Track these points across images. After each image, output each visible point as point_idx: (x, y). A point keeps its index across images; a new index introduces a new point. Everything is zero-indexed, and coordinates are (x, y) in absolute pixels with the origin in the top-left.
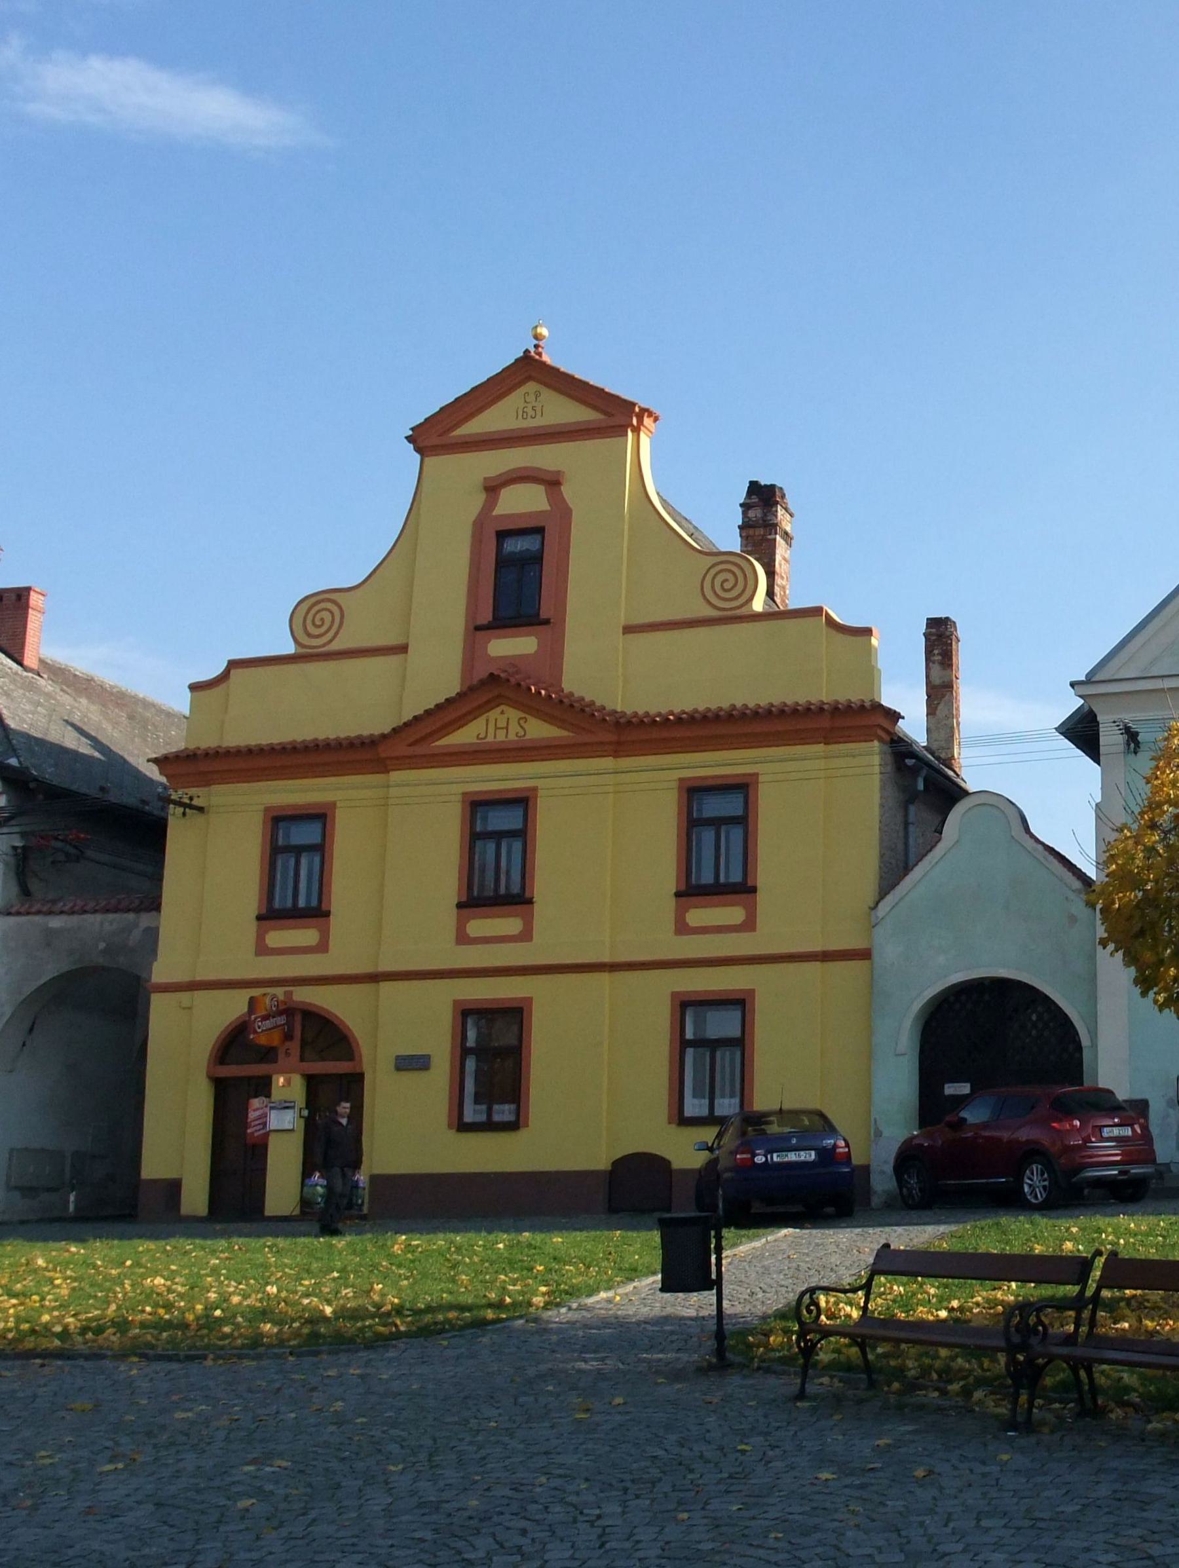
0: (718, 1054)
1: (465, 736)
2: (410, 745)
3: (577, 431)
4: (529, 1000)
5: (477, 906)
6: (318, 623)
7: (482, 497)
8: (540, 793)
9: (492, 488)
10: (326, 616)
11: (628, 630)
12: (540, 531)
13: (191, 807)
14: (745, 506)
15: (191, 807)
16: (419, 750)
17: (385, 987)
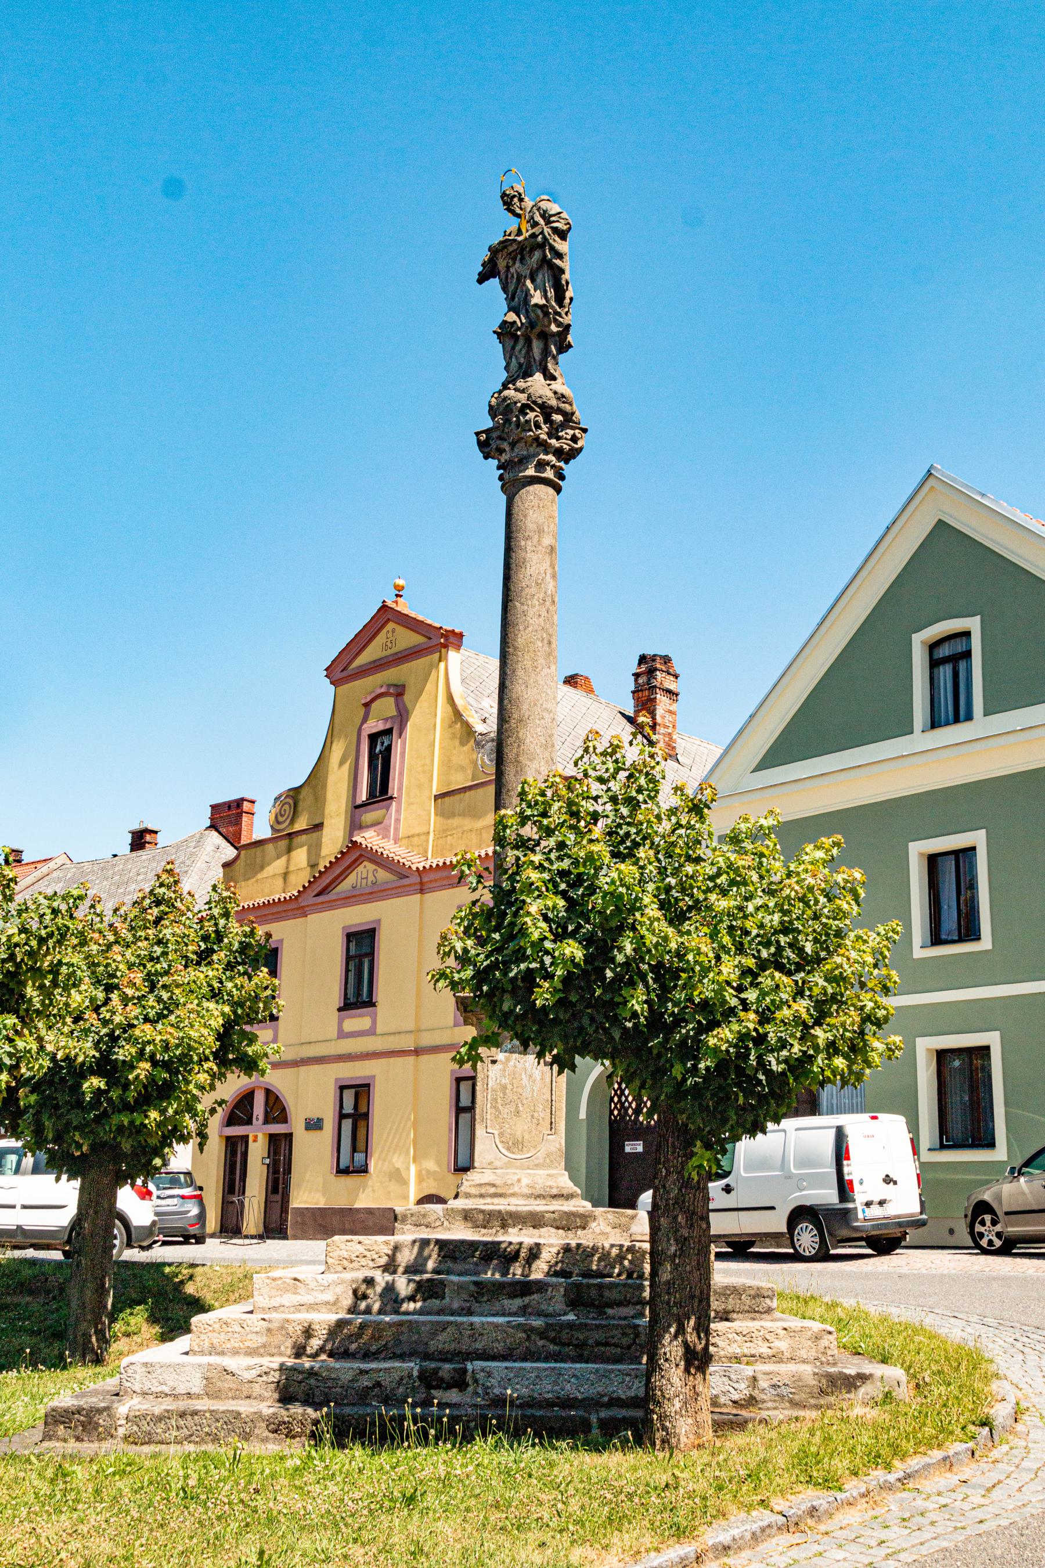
1: (346, 885)
7: (362, 710)
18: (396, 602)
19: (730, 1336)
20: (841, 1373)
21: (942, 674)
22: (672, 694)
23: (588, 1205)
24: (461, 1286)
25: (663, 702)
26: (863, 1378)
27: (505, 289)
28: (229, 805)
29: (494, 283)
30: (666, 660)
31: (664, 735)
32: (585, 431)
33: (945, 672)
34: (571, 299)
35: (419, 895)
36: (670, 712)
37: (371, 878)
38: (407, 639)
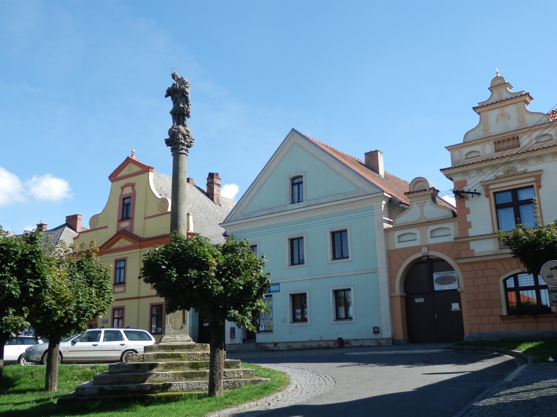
0: (120, 321)
1: (116, 246)
2: (105, 249)
3: (129, 176)
4: (125, 306)
5: (116, 285)
6: (94, 222)
7: (121, 190)
8: (128, 258)
9: (123, 188)
10: (95, 220)
11: (106, 227)
12: (130, 197)
13: (476, 193)
14: (208, 179)
15: (476, 193)
16: (107, 250)
17: (141, 300)
18: (132, 156)
19: (229, 373)
20: (255, 380)
21: (295, 188)
22: (219, 185)
23: (194, 343)
24: (162, 365)
25: (216, 188)
26: (260, 381)
27: (172, 100)
28: (72, 216)
29: (170, 98)
30: (217, 174)
31: (216, 198)
32: (194, 140)
33: (296, 187)
34: (190, 105)
35: (140, 249)
36: (218, 190)
37: (124, 243)
38: (136, 169)
